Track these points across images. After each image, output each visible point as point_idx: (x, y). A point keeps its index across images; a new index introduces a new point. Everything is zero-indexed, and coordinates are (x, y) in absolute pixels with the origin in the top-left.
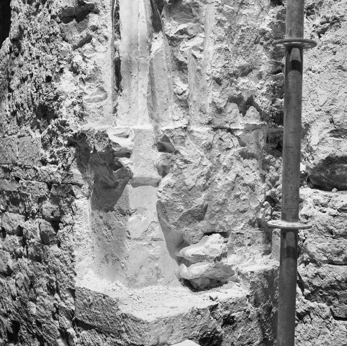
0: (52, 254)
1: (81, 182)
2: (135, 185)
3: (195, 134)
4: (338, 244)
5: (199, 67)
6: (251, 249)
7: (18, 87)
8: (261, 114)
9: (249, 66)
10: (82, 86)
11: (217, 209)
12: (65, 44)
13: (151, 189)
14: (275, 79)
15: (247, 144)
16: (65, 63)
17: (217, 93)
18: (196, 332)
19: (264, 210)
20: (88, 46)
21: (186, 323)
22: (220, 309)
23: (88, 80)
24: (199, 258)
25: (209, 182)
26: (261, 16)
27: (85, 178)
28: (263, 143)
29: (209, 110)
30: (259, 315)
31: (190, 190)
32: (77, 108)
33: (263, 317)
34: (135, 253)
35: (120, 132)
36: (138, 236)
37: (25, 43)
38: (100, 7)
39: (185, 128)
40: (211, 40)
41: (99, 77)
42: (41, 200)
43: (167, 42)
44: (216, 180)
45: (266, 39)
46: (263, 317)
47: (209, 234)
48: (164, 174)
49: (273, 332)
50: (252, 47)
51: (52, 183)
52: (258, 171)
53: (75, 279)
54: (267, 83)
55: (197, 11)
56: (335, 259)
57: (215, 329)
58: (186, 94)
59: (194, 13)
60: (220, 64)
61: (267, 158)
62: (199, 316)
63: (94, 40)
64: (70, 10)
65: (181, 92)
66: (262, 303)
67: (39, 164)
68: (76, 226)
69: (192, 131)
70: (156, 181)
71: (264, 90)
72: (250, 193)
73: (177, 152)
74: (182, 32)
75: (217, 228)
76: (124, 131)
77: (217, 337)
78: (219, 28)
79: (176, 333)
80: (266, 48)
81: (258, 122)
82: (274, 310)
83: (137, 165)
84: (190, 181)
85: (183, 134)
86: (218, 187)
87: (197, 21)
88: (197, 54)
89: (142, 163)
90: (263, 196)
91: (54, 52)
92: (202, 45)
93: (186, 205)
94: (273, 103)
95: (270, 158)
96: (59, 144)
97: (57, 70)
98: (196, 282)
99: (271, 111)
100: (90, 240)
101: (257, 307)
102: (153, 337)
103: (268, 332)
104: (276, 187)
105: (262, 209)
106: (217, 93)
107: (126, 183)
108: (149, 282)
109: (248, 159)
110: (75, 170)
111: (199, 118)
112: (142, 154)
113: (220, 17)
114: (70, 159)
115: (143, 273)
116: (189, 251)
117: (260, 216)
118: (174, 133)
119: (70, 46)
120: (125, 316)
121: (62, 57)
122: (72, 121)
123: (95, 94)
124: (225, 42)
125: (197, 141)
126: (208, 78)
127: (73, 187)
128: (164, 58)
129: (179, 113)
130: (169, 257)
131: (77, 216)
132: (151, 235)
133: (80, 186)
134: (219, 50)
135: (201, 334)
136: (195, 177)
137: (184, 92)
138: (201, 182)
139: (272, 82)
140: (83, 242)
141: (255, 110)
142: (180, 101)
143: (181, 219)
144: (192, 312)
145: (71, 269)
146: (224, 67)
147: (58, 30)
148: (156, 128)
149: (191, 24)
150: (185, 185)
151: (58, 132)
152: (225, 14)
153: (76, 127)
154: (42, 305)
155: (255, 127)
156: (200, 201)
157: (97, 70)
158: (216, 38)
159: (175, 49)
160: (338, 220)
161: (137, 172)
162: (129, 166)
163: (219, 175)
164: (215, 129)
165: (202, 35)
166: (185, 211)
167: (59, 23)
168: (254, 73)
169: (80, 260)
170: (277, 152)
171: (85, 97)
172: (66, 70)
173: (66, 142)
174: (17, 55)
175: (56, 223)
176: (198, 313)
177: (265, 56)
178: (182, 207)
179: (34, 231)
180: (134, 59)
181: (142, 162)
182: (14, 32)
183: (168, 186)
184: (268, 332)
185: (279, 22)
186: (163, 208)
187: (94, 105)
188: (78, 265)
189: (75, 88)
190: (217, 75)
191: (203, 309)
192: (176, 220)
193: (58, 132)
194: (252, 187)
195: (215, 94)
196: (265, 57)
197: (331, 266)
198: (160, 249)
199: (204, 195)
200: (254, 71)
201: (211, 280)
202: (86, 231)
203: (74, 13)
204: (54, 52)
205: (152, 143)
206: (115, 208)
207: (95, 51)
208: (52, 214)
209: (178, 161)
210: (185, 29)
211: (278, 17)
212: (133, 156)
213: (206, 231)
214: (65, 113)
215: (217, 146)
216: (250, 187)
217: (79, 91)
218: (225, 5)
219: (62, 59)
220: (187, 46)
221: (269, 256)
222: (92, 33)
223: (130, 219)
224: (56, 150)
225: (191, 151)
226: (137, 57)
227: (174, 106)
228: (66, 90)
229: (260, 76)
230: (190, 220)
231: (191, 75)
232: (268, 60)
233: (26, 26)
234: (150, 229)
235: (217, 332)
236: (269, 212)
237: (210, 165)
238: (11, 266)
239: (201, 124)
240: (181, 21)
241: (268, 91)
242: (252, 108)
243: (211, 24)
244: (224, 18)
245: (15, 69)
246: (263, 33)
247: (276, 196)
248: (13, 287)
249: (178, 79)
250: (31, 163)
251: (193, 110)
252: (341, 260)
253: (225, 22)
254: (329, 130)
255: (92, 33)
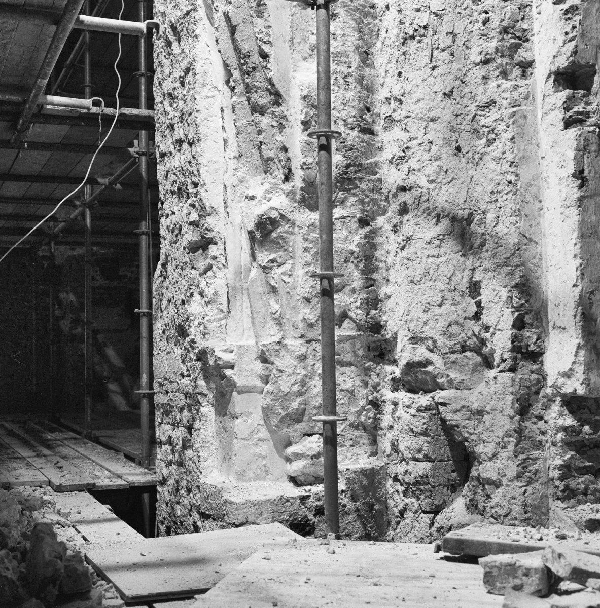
0: (187, 457)
1: (206, 391)
2: (240, 393)
3: (289, 347)
4: (418, 442)
5: (288, 290)
6: (355, 450)
7: (166, 307)
8: (357, 325)
9: (341, 283)
10: (205, 308)
11: (315, 412)
12: (193, 271)
13: (256, 396)
14: (368, 293)
15: (342, 353)
16: (194, 287)
17: (307, 311)
18: (285, 517)
19: (367, 414)
20: (210, 273)
21: (275, 508)
22: (312, 499)
23: (209, 302)
24: (299, 456)
25: (305, 388)
26: (350, 237)
27: (210, 389)
28: (361, 352)
29: (301, 325)
30: (358, 510)
31: (286, 395)
32: (202, 327)
33: (363, 513)
34: (242, 451)
35: (225, 348)
36: (245, 436)
37: (169, 268)
38: (217, 239)
39: (279, 343)
40: (300, 265)
41: (218, 300)
42: (181, 410)
43: (261, 270)
44: (312, 387)
45: (356, 258)
46: (363, 513)
47: (310, 435)
48: (267, 383)
49: (377, 529)
50: (342, 266)
51: (187, 394)
52: (358, 378)
53: (200, 476)
54: (361, 297)
55: (285, 242)
56: (418, 456)
57: (306, 516)
58: (279, 313)
59: (282, 244)
60: (309, 285)
61: (367, 365)
62: (288, 504)
63: (214, 268)
64: (195, 242)
65: (274, 311)
66: (361, 499)
67: (180, 377)
68: (202, 430)
69: (286, 345)
70: (261, 389)
71: (358, 304)
72: (350, 398)
73: (273, 363)
74: (272, 261)
75: (316, 429)
76: (228, 347)
77: (309, 524)
78: (307, 254)
79: (265, 515)
80: (356, 266)
81: (353, 333)
82: (377, 507)
83: (240, 376)
84: (285, 388)
85: (277, 347)
86: (314, 392)
87: (285, 250)
88: (286, 278)
89: (245, 373)
90: (365, 400)
91: (186, 279)
92: (291, 270)
93: (284, 409)
94: (368, 314)
95: (370, 366)
96: (191, 360)
97: (188, 295)
98: (300, 478)
99: (366, 322)
100: (215, 443)
101: (356, 502)
102: (241, 516)
103: (371, 527)
104: (378, 392)
105: (365, 413)
106: (307, 311)
107: (232, 391)
108: (257, 477)
109: (346, 366)
110: (201, 382)
111: (292, 332)
112: (243, 366)
113: (306, 244)
114: (197, 372)
115: (251, 469)
116: (290, 450)
117: (362, 419)
118: (269, 347)
119: (198, 272)
120: (225, 501)
121: (192, 283)
122: (198, 339)
123: (216, 314)
124: (313, 265)
125: (291, 353)
126: (299, 298)
127: (199, 397)
128: (258, 284)
129: (275, 329)
130: (277, 456)
131: (203, 422)
132: (258, 436)
133: (206, 395)
134: (307, 273)
135: (291, 519)
136: (289, 384)
137: (277, 311)
138: (296, 388)
139: (365, 296)
140: (208, 444)
141: (351, 321)
142: (275, 319)
143: (280, 421)
144: (281, 499)
145: (198, 468)
146: (312, 287)
147: (188, 260)
148: (257, 343)
149: (281, 253)
150: (281, 391)
151: (190, 349)
152: (311, 242)
153: (201, 344)
154: (183, 505)
155: (350, 338)
156: (295, 405)
157: (216, 294)
158: (303, 263)
159: (268, 275)
160: (416, 419)
161: (240, 381)
162: (232, 376)
163: (314, 382)
164: (308, 342)
165: (291, 262)
166: (284, 414)
167: (188, 253)
168: (347, 289)
169: (205, 460)
170: (378, 359)
171: (207, 318)
172: (195, 294)
173: (195, 358)
174: (165, 278)
175: (190, 429)
176: (288, 501)
177: (356, 273)
178: (281, 411)
179: (178, 439)
180: (238, 286)
181: (247, 372)
182: (162, 257)
183: (268, 392)
184: (371, 527)
185: (367, 242)
186: (267, 411)
187: (215, 324)
188: (203, 465)
189: (202, 310)
190: (306, 295)
191: (293, 498)
192: (277, 422)
193: (190, 349)
194: (352, 392)
195: (305, 311)
196: (356, 274)
197: (415, 462)
198: (267, 448)
199: (298, 400)
200: (347, 287)
201: (316, 478)
202: (211, 435)
203: (200, 244)
204: (186, 279)
205: (255, 356)
206: (228, 413)
207: (216, 277)
208: (188, 422)
209: (274, 371)
210: (275, 258)
211: (366, 237)
212: (236, 368)
213: (305, 432)
214: (194, 332)
215: (311, 356)
216: (349, 392)
217: (204, 313)
218: (311, 234)
219: (191, 285)
220: (277, 271)
221: (376, 457)
222: (212, 262)
223: (237, 421)
224: (189, 364)
225: (286, 362)
226: (240, 283)
227: (270, 323)
228: (195, 312)
229: (353, 291)
230: (289, 422)
231: (283, 296)
232: (359, 276)
233: (170, 253)
234: (256, 430)
235: (308, 520)
236: (372, 416)
237: (304, 373)
238: (165, 474)
239: (295, 338)
240: (271, 251)
241: (361, 304)
242: (347, 321)
243: (299, 251)
244: (310, 245)
245: (164, 291)
246: (352, 253)
247: (378, 400)
248: (166, 493)
249: (273, 300)
250: (174, 377)
251: (288, 327)
252: (421, 457)
253: (312, 248)
254: (408, 338)
255: (212, 262)
